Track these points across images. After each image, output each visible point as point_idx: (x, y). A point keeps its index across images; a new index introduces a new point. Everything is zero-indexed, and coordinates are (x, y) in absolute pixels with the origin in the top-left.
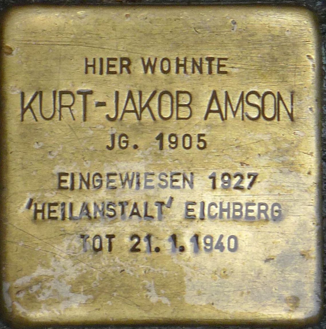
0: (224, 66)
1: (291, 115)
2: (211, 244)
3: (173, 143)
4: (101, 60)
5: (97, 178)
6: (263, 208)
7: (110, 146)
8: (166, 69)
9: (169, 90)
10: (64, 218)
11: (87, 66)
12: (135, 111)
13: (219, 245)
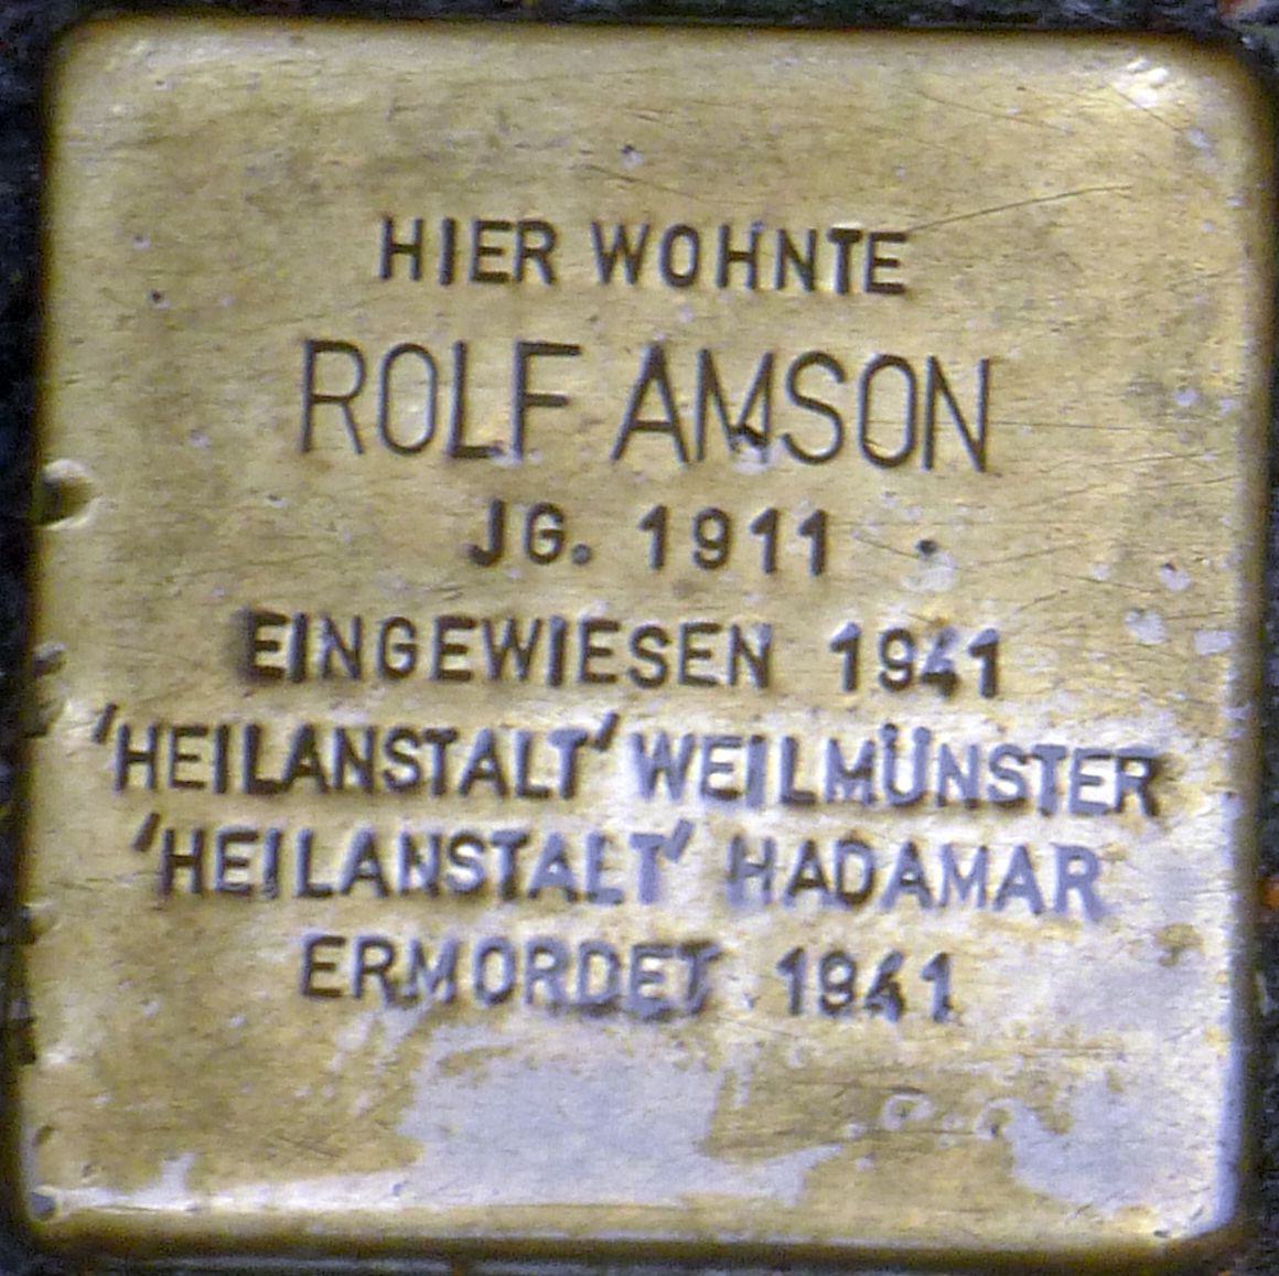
0: (893, 263)
1: (978, 450)
3: (708, 544)
4: (450, 228)
7: (486, 546)
8: (682, 269)
9: (837, 355)
10: (222, 785)
11: (392, 249)
12: (673, 426)
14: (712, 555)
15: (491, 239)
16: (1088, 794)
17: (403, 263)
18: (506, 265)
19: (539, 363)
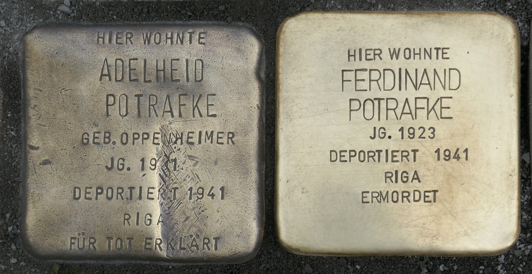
2: (449, 155)
5: (382, 130)
7: (373, 136)
11: (349, 56)
13: (456, 156)
14: (411, 136)
15: (368, 52)
17: (352, 58)
18: (372, 56)
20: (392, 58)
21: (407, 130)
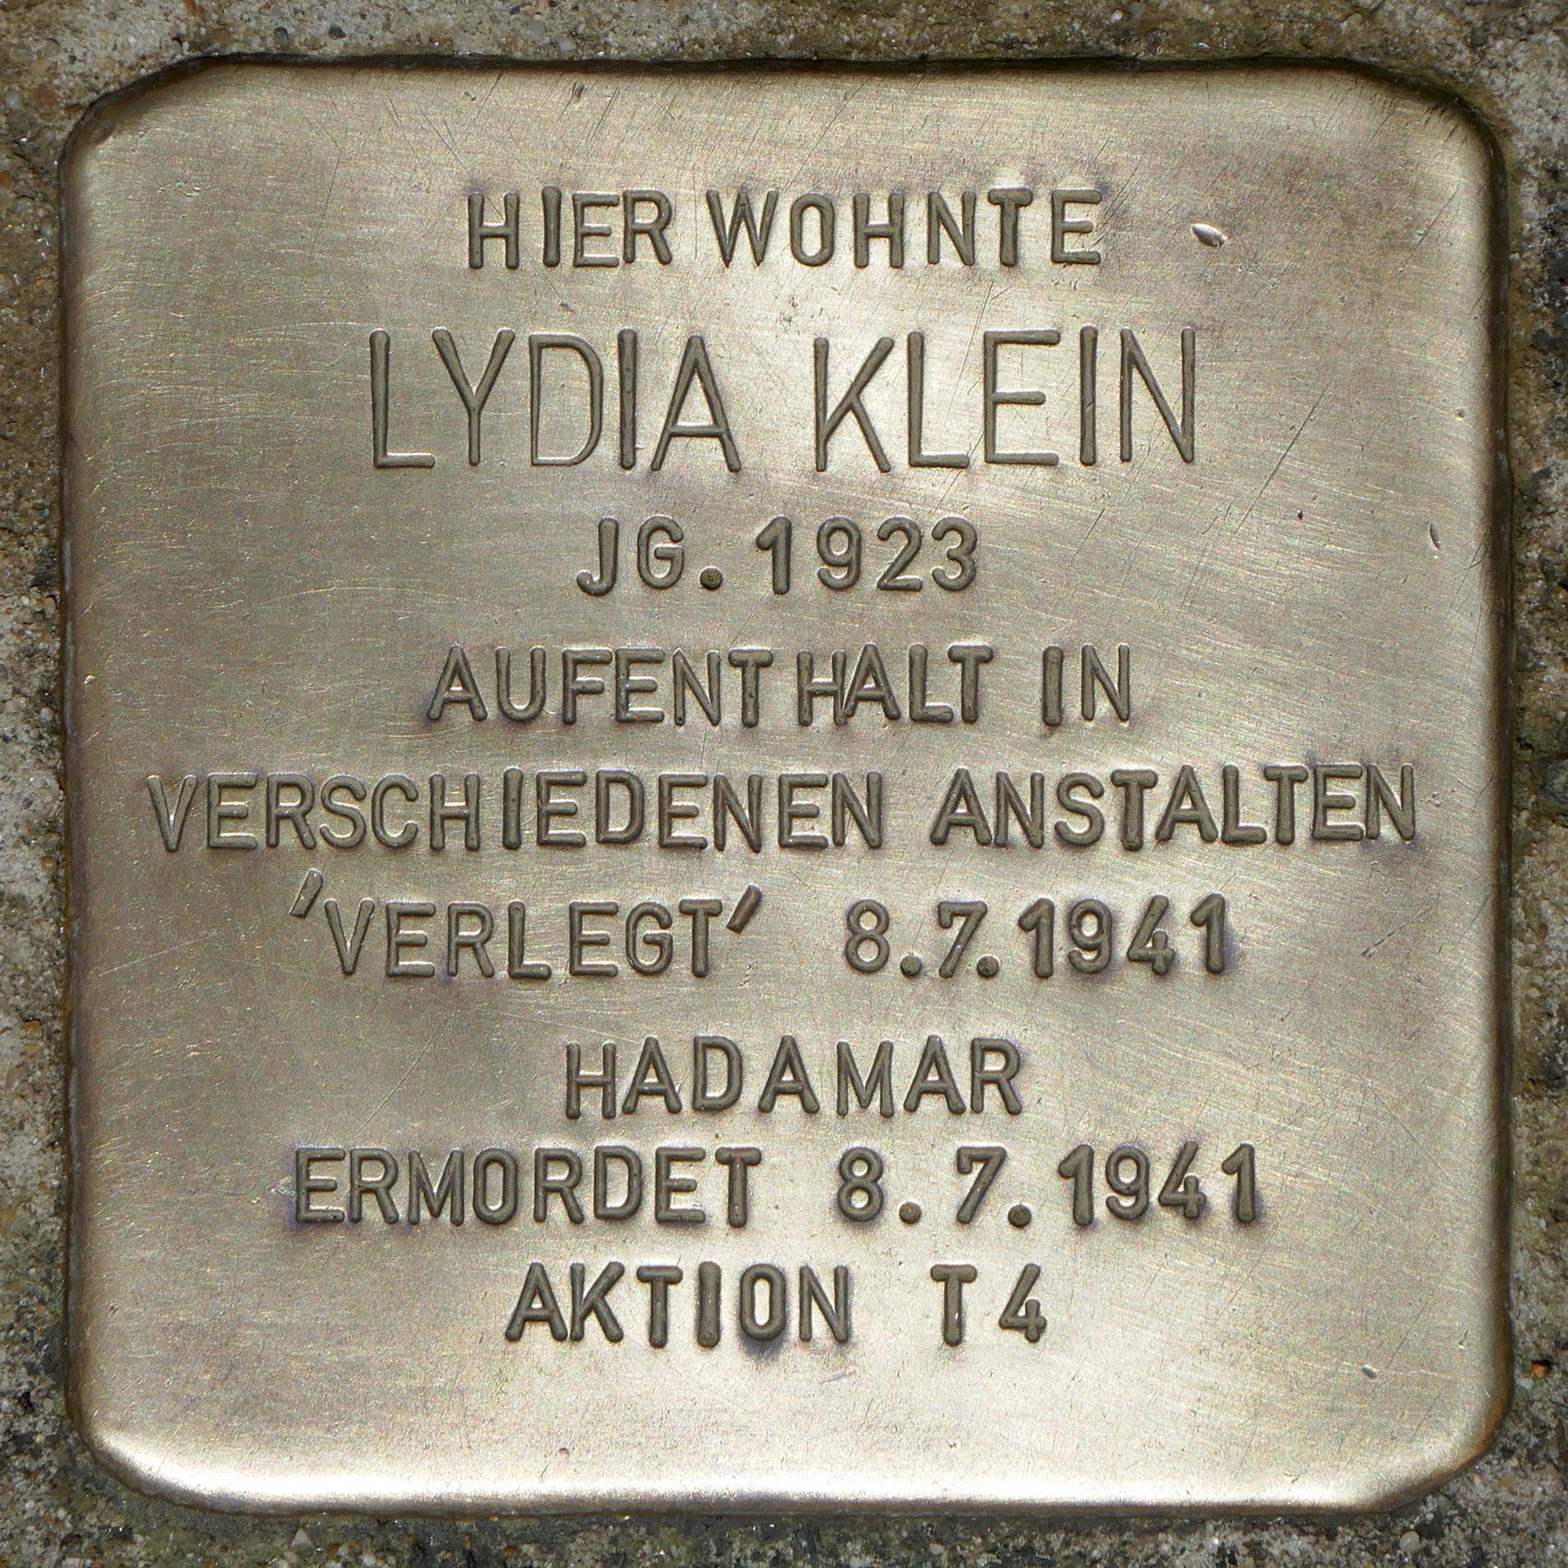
6: (470, 930)
16: (1335, 820)
18: (821, 829)
19: (1007, 357)
20: (727, 259)
21: (812, 546)
